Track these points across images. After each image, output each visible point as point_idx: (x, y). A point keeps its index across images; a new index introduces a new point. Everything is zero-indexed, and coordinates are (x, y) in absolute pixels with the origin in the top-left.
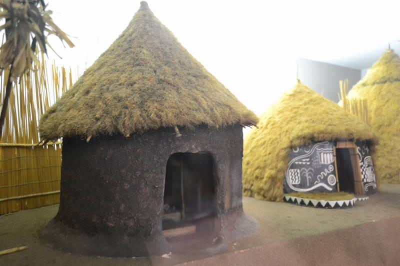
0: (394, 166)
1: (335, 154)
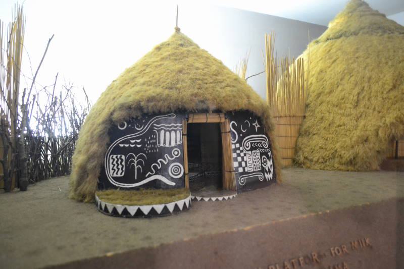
0: (330, 146)
1: (185, 133)
